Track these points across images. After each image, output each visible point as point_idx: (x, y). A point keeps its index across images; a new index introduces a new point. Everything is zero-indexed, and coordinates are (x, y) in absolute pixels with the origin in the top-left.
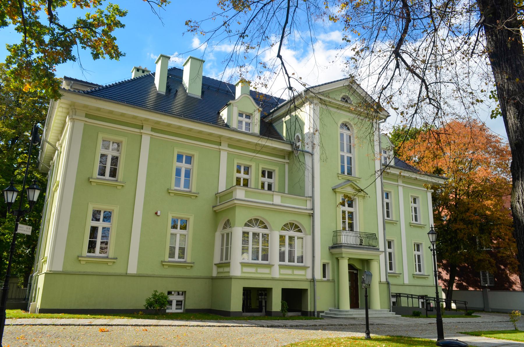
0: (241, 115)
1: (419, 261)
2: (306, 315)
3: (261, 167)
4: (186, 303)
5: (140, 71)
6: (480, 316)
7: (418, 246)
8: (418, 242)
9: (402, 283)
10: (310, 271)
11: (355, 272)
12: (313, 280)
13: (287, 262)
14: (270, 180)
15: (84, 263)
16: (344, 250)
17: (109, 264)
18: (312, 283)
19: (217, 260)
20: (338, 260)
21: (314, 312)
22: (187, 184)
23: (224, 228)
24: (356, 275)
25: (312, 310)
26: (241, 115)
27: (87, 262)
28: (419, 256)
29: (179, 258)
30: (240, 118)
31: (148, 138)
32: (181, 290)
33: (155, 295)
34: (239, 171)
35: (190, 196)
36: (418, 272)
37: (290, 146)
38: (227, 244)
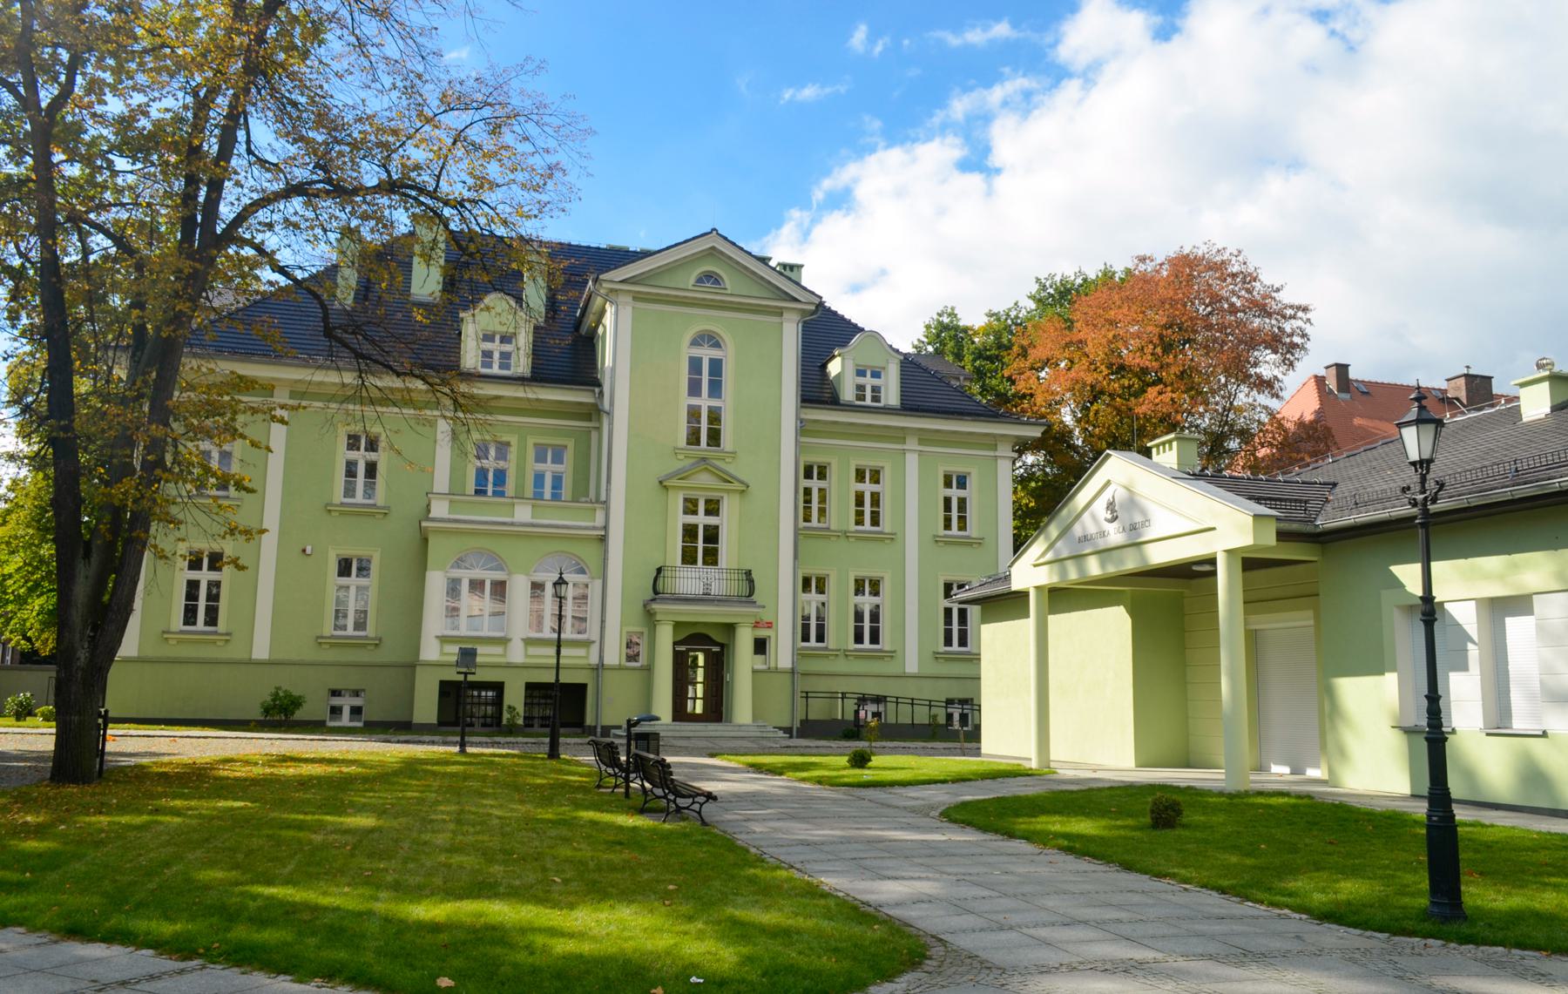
0: (861, 373)
9: (898, 671)
10: (595, 649)
11: (716, 649)
17: (219, 643)
21: (595, 727)
22: (370, 488)
25: (593, 724)
27: (180, 641)
29: (206, 624)
30: (861, 380)
31: (916, 456)
33: (276, 696)
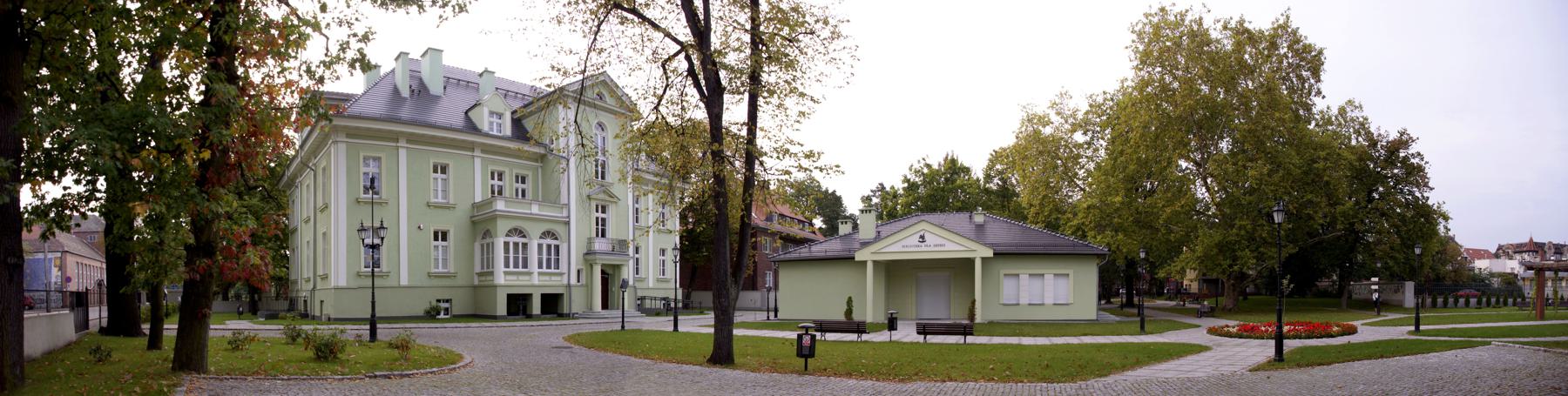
1: (664, 266)
2: (561, 316)
3: (515, 171)
6: (1489, 343)
7: (663, 251)
8: (664, 247)
10: (566, 276)
12: (569, 286)
13: (511, 269)
14: (524, 186)
16: (598, 256)
19: (478, 269)
20: (591, 266)
23: (483, 238)
24: (607, 279)
28: (664, 261)
32: (447, 297)
34: (493, 178)
35: (449, 208)
36: (662, 277)
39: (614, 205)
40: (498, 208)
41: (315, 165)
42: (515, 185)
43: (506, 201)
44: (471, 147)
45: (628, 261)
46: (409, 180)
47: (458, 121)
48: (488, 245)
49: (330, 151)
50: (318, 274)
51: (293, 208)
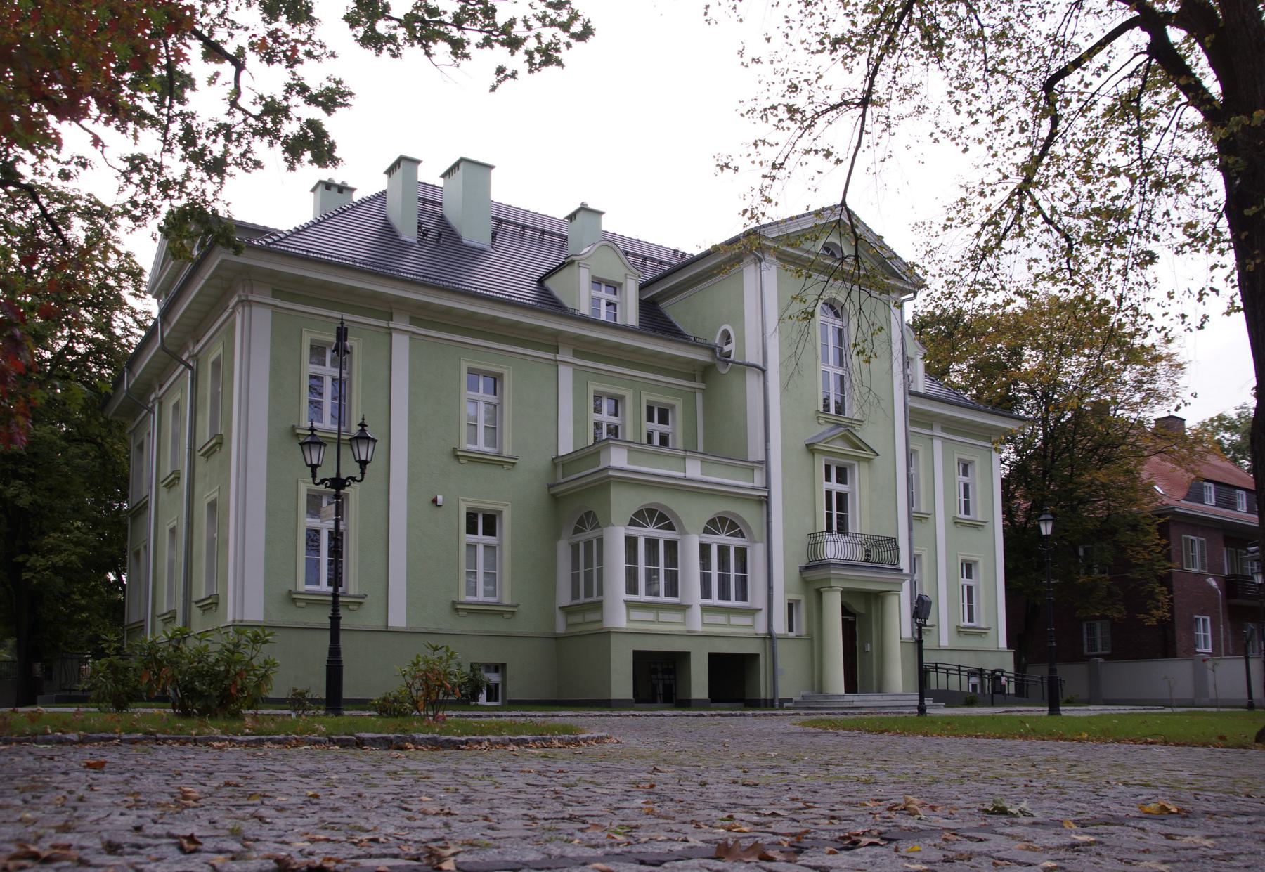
2: (755, 704)
3: (645, 398)
4: (508, 688)
5: (332, 188)
8: (970, 557)
10: (762, 617)
15: (303, 604)
18: (768, 641)
19: (564, 598)
20: (819, 594)
23: (577, 531)
26: (597, 282)
34: (598, 410)
35: (500, 464)
37: (708, 353)
38: (588, 563)
39: (864, 465)
40: (614, 463)
41: (194, 357)
42: (647, 426)
43: (630, 450)
44: (552, 342)
45: (900, 583)
46: (413, 395)
47: (525, 291)
48: (588, 544)
49: (235, 319)
50: (195, 598)
51: (140, 459)
